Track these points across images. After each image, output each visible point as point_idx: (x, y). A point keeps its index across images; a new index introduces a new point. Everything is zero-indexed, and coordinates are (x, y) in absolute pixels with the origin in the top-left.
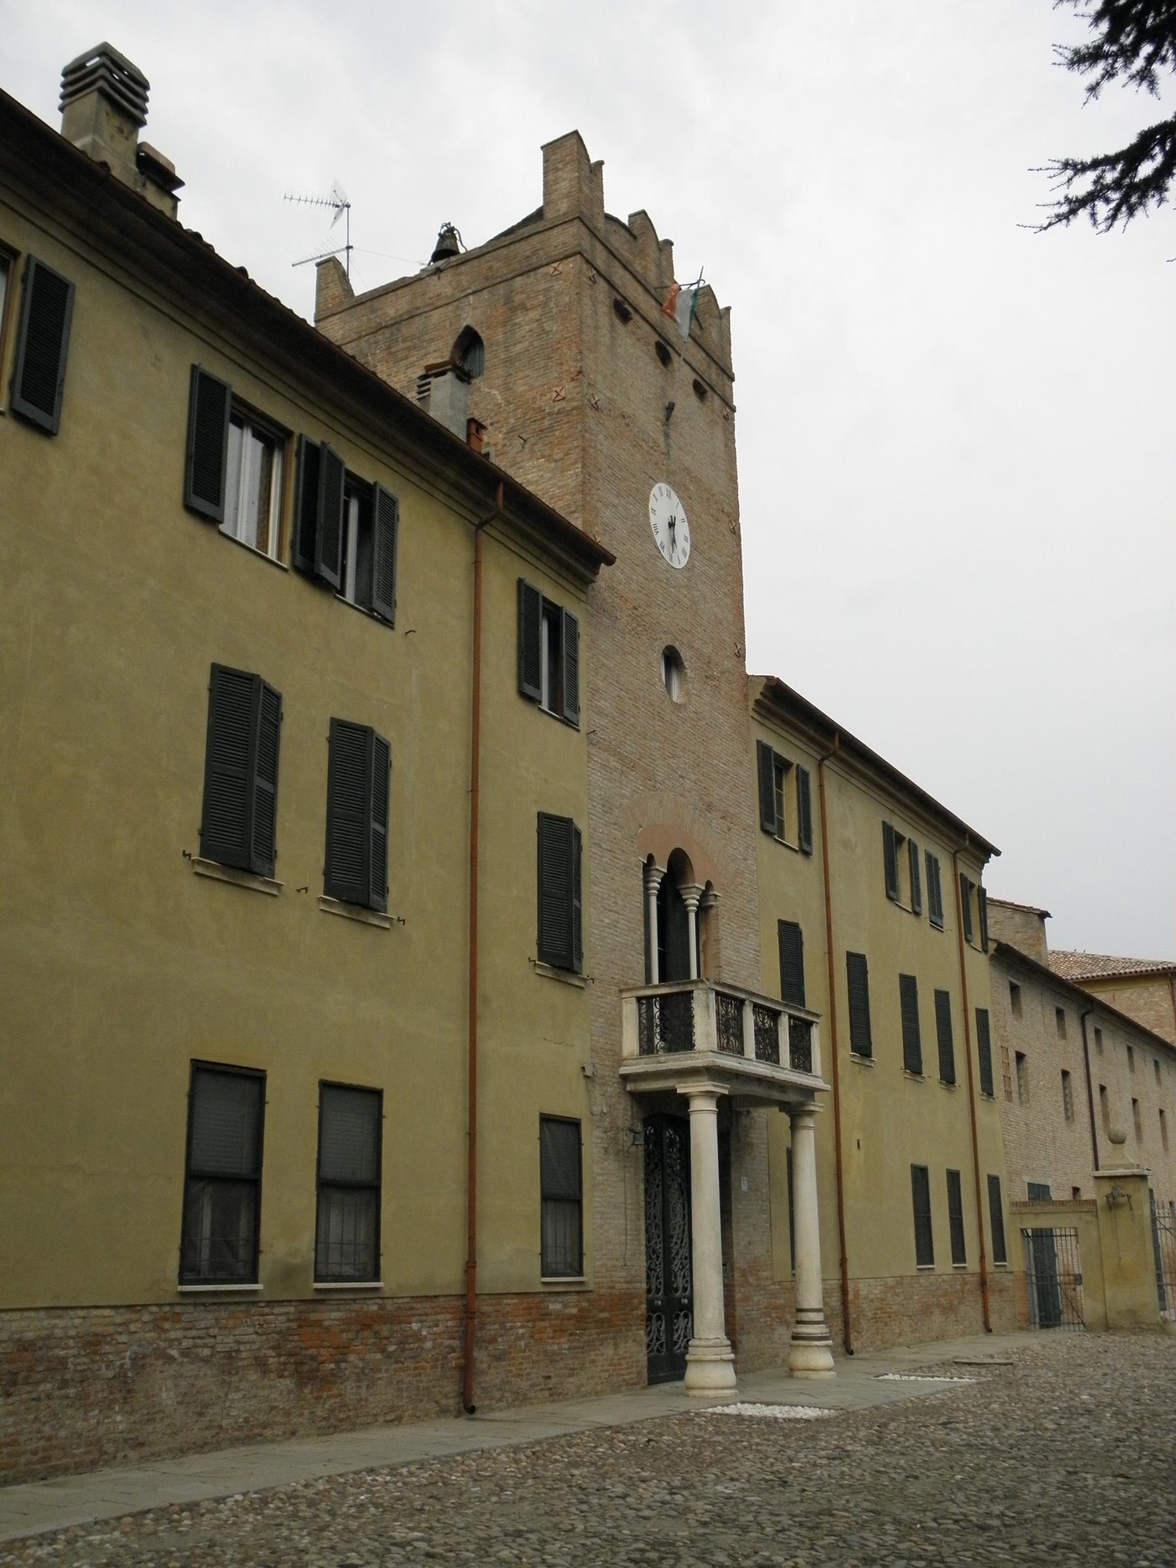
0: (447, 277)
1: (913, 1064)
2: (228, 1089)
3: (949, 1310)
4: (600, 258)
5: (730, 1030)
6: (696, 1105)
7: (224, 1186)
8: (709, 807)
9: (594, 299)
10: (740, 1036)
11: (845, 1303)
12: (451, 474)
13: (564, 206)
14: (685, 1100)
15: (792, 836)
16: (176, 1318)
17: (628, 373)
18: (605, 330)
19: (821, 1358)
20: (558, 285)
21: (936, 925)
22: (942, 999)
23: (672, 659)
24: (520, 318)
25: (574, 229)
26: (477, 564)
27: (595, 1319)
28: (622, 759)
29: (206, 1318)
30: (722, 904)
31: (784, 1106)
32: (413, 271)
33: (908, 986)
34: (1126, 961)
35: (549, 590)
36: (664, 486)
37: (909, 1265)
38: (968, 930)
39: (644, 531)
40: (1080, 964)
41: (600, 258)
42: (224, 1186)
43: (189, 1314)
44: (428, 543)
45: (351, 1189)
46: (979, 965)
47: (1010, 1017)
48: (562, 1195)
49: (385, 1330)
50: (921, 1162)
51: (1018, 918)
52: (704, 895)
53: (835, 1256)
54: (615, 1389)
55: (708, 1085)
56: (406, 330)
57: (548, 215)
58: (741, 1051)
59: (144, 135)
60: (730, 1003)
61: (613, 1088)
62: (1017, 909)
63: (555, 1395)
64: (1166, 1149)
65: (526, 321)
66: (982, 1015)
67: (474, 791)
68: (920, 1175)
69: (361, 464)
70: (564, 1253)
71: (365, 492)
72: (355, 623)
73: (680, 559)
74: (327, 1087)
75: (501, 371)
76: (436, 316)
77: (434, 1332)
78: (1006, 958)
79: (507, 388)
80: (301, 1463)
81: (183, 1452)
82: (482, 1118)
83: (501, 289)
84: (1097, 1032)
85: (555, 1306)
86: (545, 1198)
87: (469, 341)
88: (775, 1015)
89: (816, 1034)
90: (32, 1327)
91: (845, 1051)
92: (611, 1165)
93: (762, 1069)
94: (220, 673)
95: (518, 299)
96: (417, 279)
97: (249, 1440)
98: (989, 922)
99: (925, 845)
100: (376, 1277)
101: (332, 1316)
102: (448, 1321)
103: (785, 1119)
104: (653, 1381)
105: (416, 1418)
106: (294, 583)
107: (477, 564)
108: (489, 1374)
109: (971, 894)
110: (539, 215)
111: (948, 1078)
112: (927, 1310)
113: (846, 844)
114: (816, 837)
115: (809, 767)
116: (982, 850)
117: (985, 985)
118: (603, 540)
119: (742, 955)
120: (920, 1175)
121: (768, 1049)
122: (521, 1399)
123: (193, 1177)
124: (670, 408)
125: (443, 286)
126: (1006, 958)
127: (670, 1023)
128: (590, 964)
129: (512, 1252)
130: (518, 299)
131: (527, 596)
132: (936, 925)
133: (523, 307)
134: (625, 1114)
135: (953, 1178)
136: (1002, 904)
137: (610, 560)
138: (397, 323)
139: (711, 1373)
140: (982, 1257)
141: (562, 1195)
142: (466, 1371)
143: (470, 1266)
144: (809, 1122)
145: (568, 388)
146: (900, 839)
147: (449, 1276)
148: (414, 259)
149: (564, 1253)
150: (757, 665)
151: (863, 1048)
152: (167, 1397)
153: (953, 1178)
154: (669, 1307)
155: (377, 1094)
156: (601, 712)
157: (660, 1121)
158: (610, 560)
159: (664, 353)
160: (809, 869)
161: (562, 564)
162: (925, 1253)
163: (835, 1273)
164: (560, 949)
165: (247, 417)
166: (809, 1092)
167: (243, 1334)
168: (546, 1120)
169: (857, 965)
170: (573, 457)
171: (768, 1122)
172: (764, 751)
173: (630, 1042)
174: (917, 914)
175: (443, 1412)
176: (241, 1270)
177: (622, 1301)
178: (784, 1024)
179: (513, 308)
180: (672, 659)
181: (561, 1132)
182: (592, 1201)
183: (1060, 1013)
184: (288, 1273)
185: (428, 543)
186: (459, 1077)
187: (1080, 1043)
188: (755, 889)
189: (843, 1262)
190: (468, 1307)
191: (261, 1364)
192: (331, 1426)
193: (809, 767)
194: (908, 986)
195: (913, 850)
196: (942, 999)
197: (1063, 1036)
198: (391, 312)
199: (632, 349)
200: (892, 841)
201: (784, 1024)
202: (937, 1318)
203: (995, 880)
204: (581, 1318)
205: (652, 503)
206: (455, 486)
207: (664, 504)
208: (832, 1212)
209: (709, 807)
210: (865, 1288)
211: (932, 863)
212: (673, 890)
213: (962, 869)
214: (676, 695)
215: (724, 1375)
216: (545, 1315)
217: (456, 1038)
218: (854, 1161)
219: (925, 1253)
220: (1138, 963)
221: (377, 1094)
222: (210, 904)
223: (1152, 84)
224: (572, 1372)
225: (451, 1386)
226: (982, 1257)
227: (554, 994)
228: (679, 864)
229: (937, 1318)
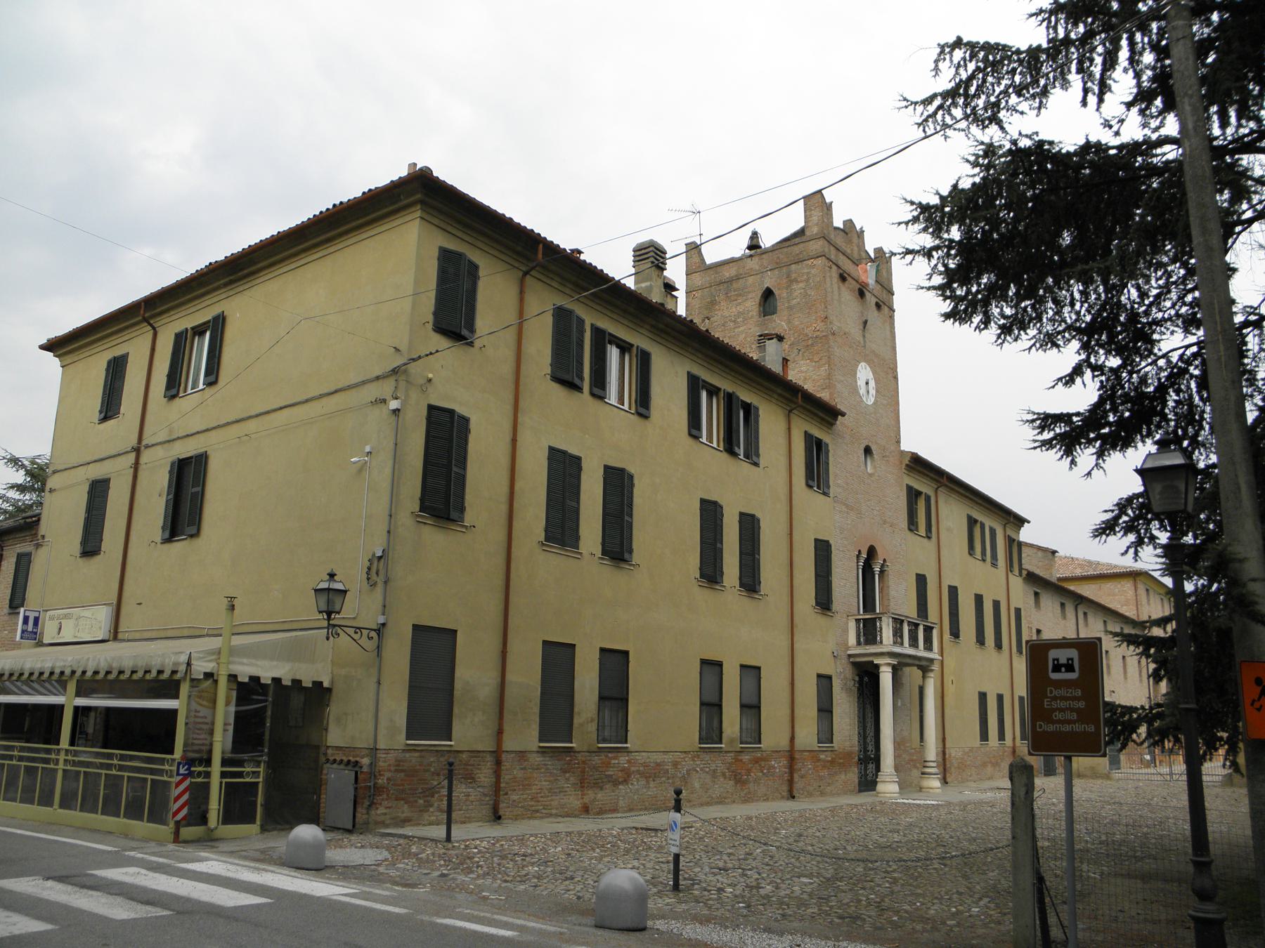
0: (756, 259)
1: (981, 640)
2: (712, 667)
3: (995, 765)
4: (833, 254)
5: (898, 633)
6: (882, 669)
7: (712, 707)
8: (885, 522)
9: (831, 277)
10: (902, 637)
11: (944, 759)
12: (779, 391)
13: (815, 230)
14: (877, 666)
15: (922, 531)
16: (698, 757)
17: (846, 309)
18: (835, 286)
19: (935, 783)
20: (813, 271)
21: (994, 565)
22: (996, 605)
23: (868, 451)
24: (794, 286)
25: (821, 242)
26: (789, 429)
27: (838, 762)
28: (847, 506)
29: (707, 757)
30: (891, 569)
31: (920, 667)
32: (738, 254)
33: (979, 599)
34: (1109, 565)
35: (817, 433)
36: (863, 364)
37: (977, 742)
38: (1011, 566)
39: (855, 390)
40: (1081, 566)
41: (833, 254)
42: (712, 707)
43: (703, 755)
44: (772, 423)
45: (751, 708)
46: (1017, 583)
47: (1033, 610)
48: (825, 710)
49: (763, 763)
50: (983, 690)
51: (1040, 554)
52: (883, 566)
53: (941, 737)
54: (845, 793)
55: (889, 661)
56: (735, 285)
57: (808, 233)
58: (902, 644)
59: (665, 273)
60: (898, 622)
61: (845, 661)
62: (1039, 548)
63: (822, 794)
64: (1126, 678)
65: (798, 288)
66: (1018, 611)
67: (791, 534)
68: (983, 697)
69: (745, 396)
70: (826, 735)
71: (747, 408)
72: (746, 467)
73: (870, 400)
74: (742, 666)
75: (786, 312)
76: (751, 279)
77: (779, 765)
78: (1032, 578)
79: (789, 322)
80: (738, 812)
81: (702, 805)
82: (796, 677)
83: (784, 270)
84: (1085, 614)
85: (822, 757)
86: (819, 710)
87: (768, 294)
88: (917, 625)
89: (935, 633)
90: (659, 758)
91: (947, 636)
92: (844, 695)
93: (911, 651)
94: (703, 501)
95: (794, 276)
96: (740, 259)
97: (721, 803)
98: (1023, 555)
99: (989, 522)
100: (760, 742)
101: (746, 758)
102: (784, 762)
103: (920, 673)
104: (860, 791)
105: (773, 799)
106: (725, 456)
107: (789, 429)
108: (799, 784)
109: (1015, 546)
110: (801, 232)
111: (999, 646)
112: (984, 765)
113: (948, 529)
114: (934, 529)
115: (931, 493)
116: (1020, 521)
117: (1020, 594)
118: (840, 407)
119: (899, 596)
120: (983, 697)
121: (914, 642)
122: (810, 795)
123: (702, 704)
124: (865, 322)
125: (754, 264)
126: (1032, 578)
127: (869, 632)
128: (836, 606)
129: (807, 735)
130: (794, 276)
131: (808, 436)
132: (994, 565)
133: (797, 282)
134: (849, 672)
135: (1000, 698)
136: (1032, 546)
137: (843, 415)
138: (730, 281)
139: (888, 787)
140: (1014, 738)
141: (825, 710)
142: (791, 782)
143: (792, 739)
144: (931, 674)
145: (820, 326)
146: (976, 521)
147: (784, 743)
148: (736, 247)
149: (826, 735)
150: (908, 445)
151: (955, 634)
152: (697, 785)
153: (1000, 698)
154: (869, 759)
155: (759, 668)
156: (839, 486)
157: (866, 677)
158: (843, 415)
159: (861, 294)
160: (930, 546)
161: (823, 419)
162: (984, 736)
163: (941, 746)
164: (824, 602)
165: (713, 391)
166: (931, 661)
167: (718, 764)
168: (819, 676)
169: (953, 591)
170: (823, 361)
171: (913, 674)
172: (910, 489)
173: (852, 640)
174: (984, 560)
175: (783, 797)
176: (716, 739)
177: (849, 755)
178: (921, 628)
179: (791, 281)
180: (868, 451)
181: (825, 681)
182: (837, 711)
183: (1063, 605)
184: (732, 741)
185: (772, 423)
186: (787, 660)
187: (1074, 620)
188: (906, 555)
189: (944, 740)
190: (791, 756)
191: (724, 774)
192: (747, 800)
193: (931, 493)
194: (979, 599)
195: (983, 526)
196: (996, 605)
197: (1064, 617)
198: (727, 275)
199: (847, 295)
200: (972, 522)
201: (921, 628)
202: (989, 769)
203: (1026, 535)
204: (832, 762)
205: (858, 375)
206: (780, 395)
207: (864, 373)
208: (940, 714)
209: (885, 522)
210: (954, 752)
211: (993, 532)
212: (870, 567)
213: (1009, 532)
214: (870, 470)
215: (895, 788)
216: (819, 760)
217: (786, 643)
218: (950, 690)
219: (984, 736)
220: (1116, 566)
221: (759, 668)
222: (702, 596)
223: (1129, 110)
224: (829, 785)
225: (785, 788)
226: (1014, 738)
227: (822, 620)
228: (872, 552)
229: (989, 769)
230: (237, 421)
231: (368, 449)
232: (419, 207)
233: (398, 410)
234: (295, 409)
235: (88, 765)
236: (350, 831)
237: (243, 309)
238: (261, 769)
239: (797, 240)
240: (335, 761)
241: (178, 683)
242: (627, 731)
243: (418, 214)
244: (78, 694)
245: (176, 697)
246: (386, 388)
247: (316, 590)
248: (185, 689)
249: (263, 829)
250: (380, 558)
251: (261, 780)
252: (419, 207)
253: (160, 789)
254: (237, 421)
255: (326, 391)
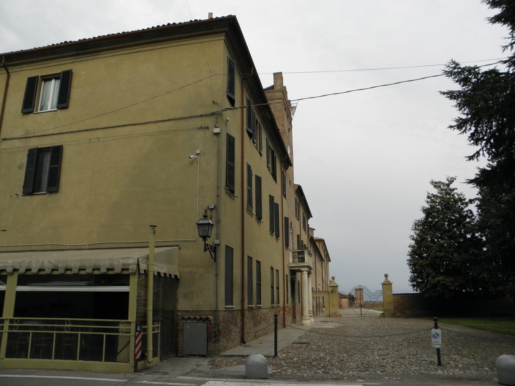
57: (275, 88)
100: (260, 304)
140: (243, 301)
226: (243, 301)
230: (86, 130)
231: (198, 152)
232: (224, 34)
233: (219, 133)
234: (136, 127)
235: (36, 328)
236: (204, 356)
237: (83, 70)
238: (159, 325)
239: (270, 91)
240: (189, 318)
241: (128, 277)
242: (261, 299)
243: (223, 37)
244: (20, 283)
245: (127, 284)
246: (209, 122)
247: (198, 224)
248: (134, 280)
249: (161, 360)
250: (212, 209)
251: (159, 331)
252: (224, 34)
253: (113, 342)
254: (86, 130)
255: (152, 120)
